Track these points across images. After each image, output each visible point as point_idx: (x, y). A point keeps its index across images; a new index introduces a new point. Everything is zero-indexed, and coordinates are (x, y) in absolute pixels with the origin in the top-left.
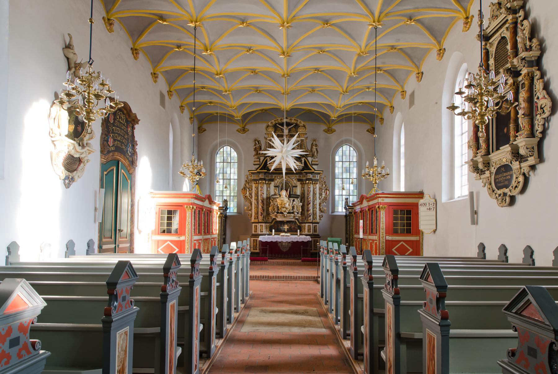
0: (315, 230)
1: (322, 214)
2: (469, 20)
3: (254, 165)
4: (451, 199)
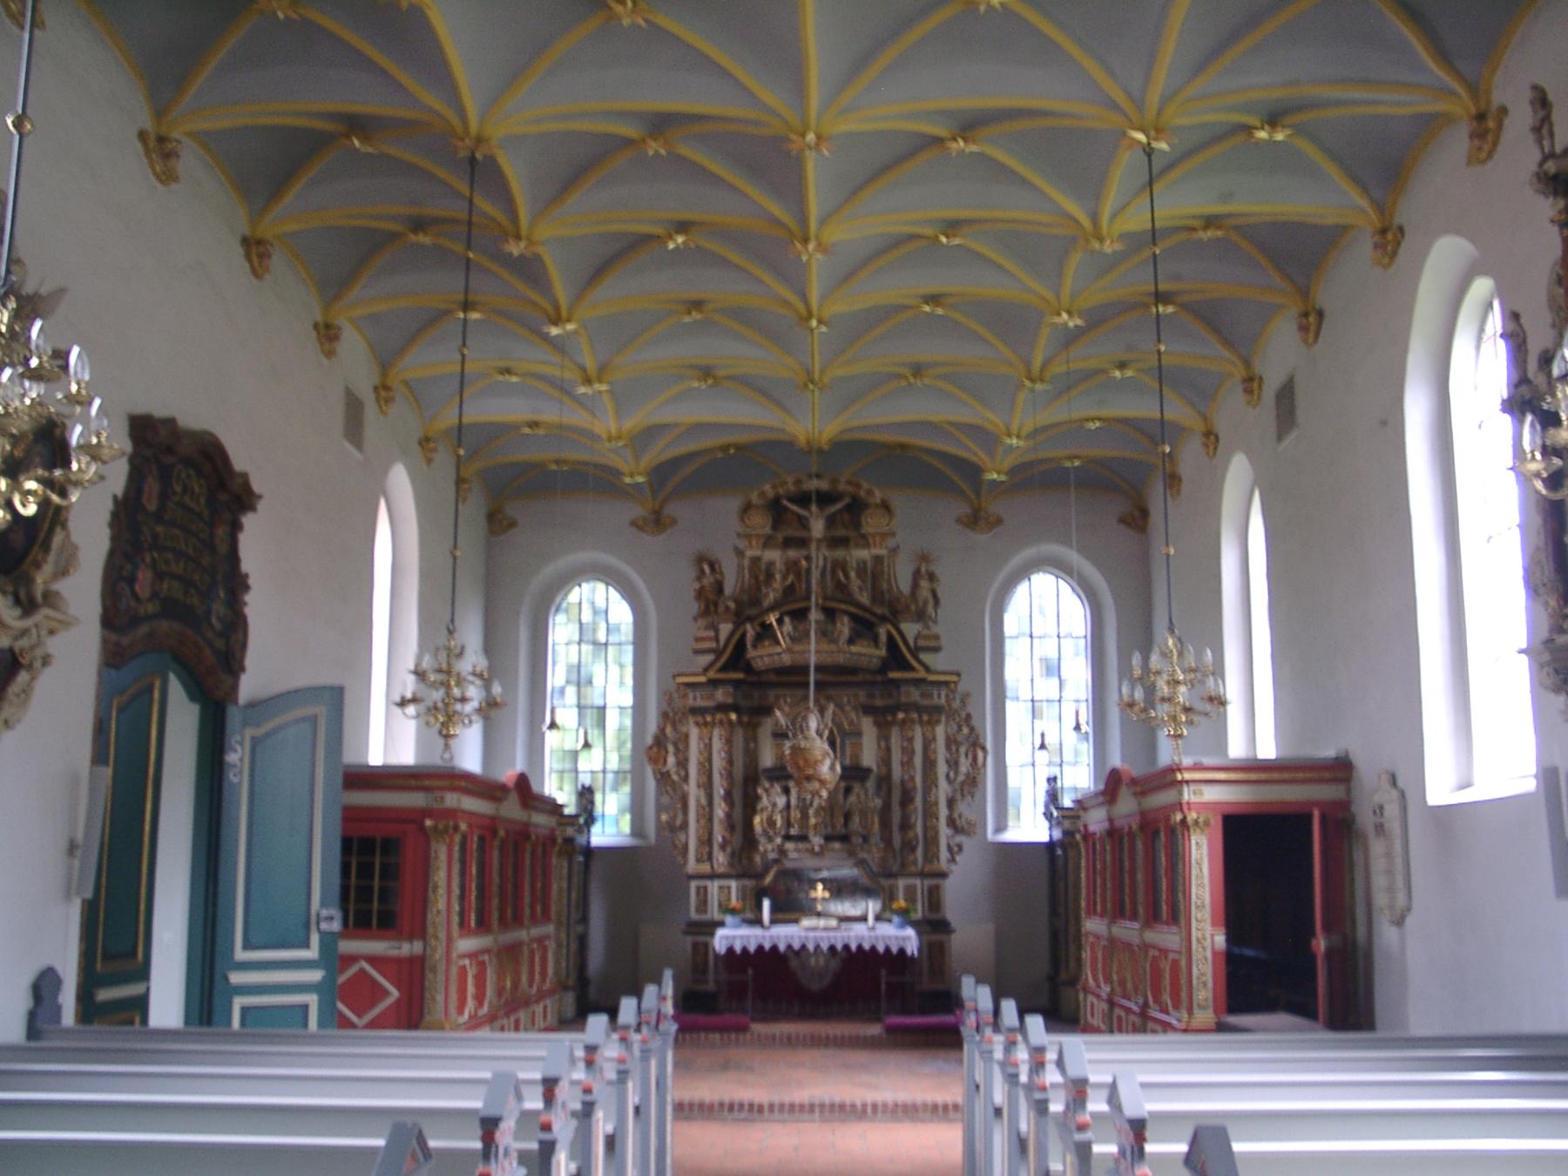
1: (959, 839)
2: (1491, 124)
3: (697, 652)
4: (1466, 785)
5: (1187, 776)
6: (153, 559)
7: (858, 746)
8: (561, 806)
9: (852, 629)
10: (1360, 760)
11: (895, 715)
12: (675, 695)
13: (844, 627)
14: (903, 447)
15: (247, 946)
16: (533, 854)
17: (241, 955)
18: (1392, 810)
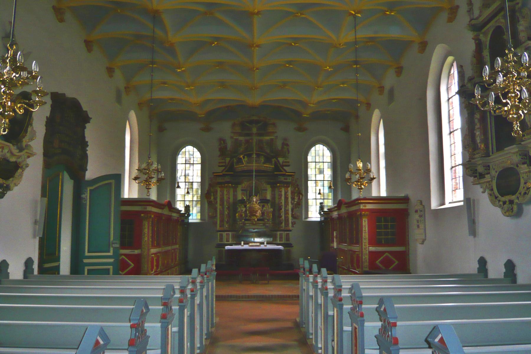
0: (288, 238)
1: (294, 220)
3: (219, 166)
8: (181, 211)
10: (411, 197)
13: (262, 159)
15: (89, 252)
17: (87, 254)
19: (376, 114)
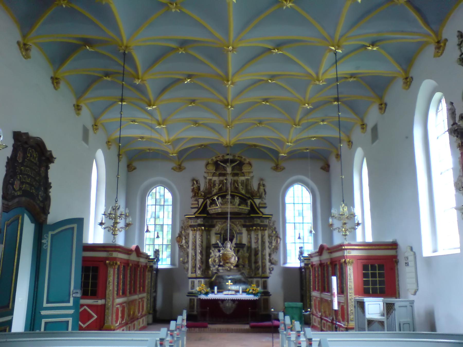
1: (273, 266)
2: (442, 44)
3: (192, 208)
4: (435, 251)
5: (346, 247)
6: (20, 177)
7: (241, 238)
8: (149, 256)
9: (239, 201)
11: (252, 227)
12: (185, 221)
13: (237, 200)
14: (255, 146)
15: (48, 302)
16: (140, 271)
17: (45, 305)
18: (411, 258)
19: (359, 153)
